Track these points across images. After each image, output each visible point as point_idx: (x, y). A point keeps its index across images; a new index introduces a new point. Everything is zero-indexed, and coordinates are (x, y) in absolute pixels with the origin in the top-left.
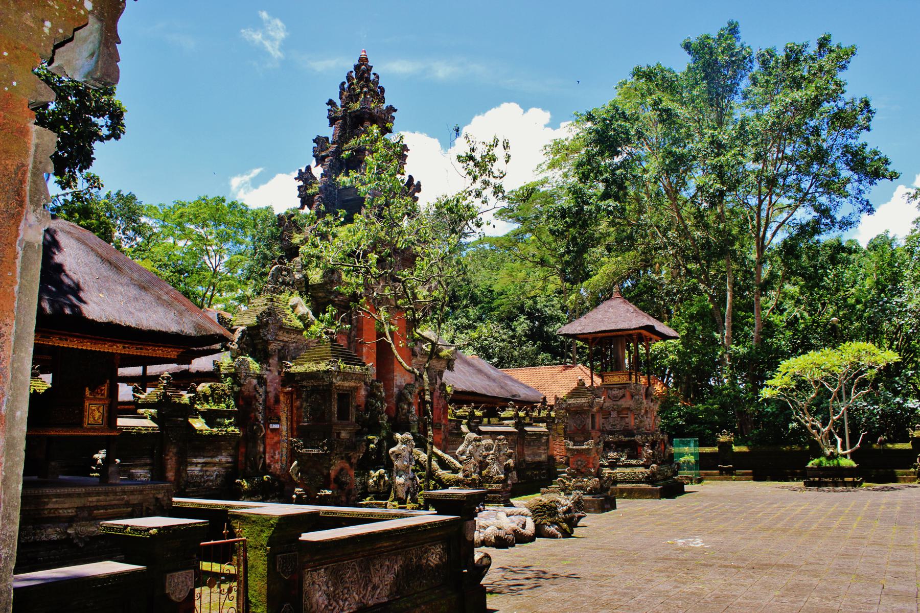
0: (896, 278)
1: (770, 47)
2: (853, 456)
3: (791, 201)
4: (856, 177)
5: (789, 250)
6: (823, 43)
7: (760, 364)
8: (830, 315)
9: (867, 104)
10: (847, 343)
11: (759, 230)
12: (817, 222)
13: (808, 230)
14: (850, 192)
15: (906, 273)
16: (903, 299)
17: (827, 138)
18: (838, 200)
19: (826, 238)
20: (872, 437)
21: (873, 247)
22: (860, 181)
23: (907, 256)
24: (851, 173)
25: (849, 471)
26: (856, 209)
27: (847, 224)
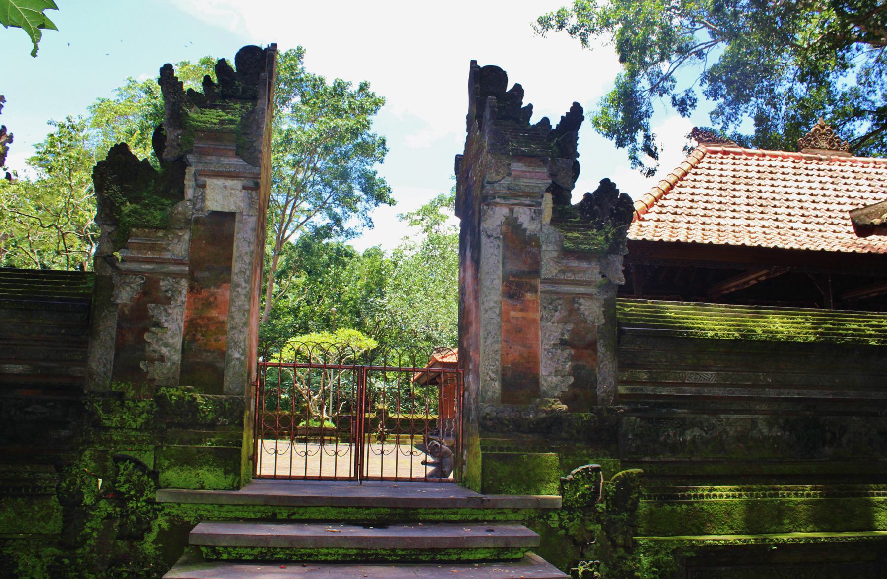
0: (380, 283)
1: (323, 76)
2: (334, 421)
3: (311, 206)
4: (365, 197)
5: (306, 247)
6: (363, 87)
7: (271, 340)
8: (327, 305)
9: (384, 142)
10: (342, 329)
11: (281, 225)
12: (329, 228)
13: (322, 233)
14: (359, 208)
15: (390, 280)
16: (385, 301)
17: (354, 163)
18: (349, 213)
19: (334, 241)
20: (347, 408)
21: (368, 254)
22: (367, 202)
23: (392, 267)
24: (362, 193)
25: (330, 432)
26: (360, 223)
27: (350, 234)
